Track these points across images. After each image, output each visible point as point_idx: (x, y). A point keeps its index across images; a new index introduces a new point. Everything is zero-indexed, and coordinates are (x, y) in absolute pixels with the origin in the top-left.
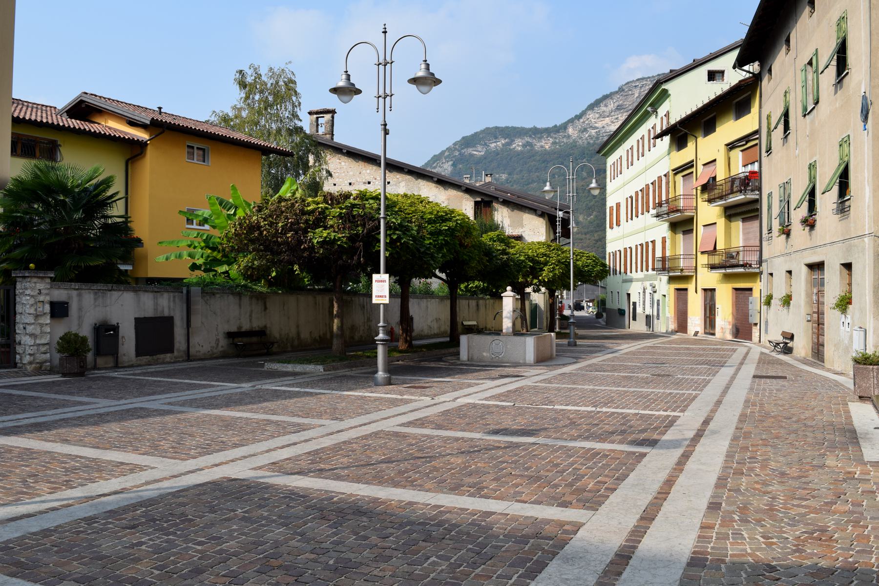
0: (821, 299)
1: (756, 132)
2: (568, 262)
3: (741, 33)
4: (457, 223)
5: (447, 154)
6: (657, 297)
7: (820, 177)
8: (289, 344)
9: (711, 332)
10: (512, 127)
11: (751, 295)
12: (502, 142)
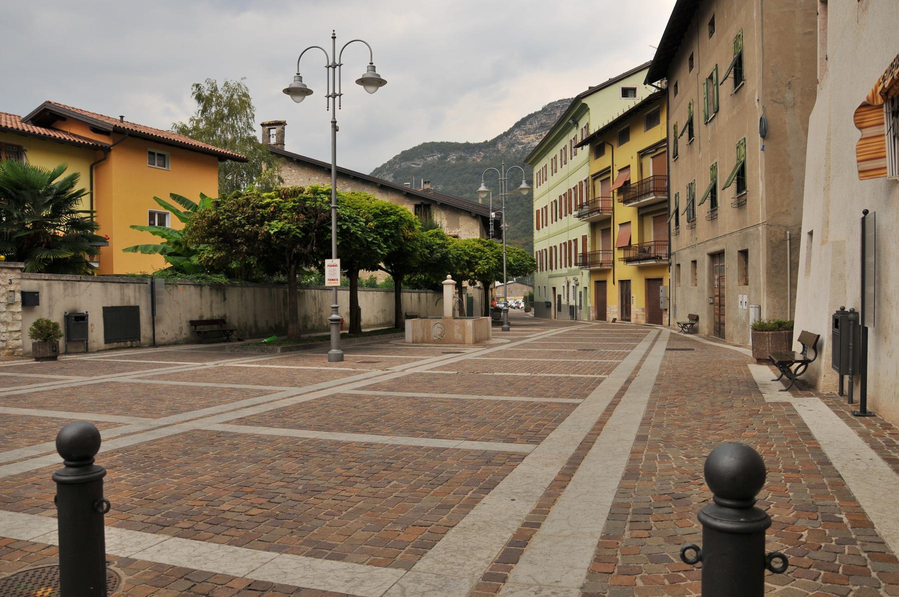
0: (722, 284)
1: (666, 140)
2: (501, 257)
3: (649, 55)
5: (387, 166)
6: (579, 289)
7: (720, 176)
8: (247, 332)
9: (627, 318)
10: (447, 142)
11: (662, 284)
12: (437, 156)
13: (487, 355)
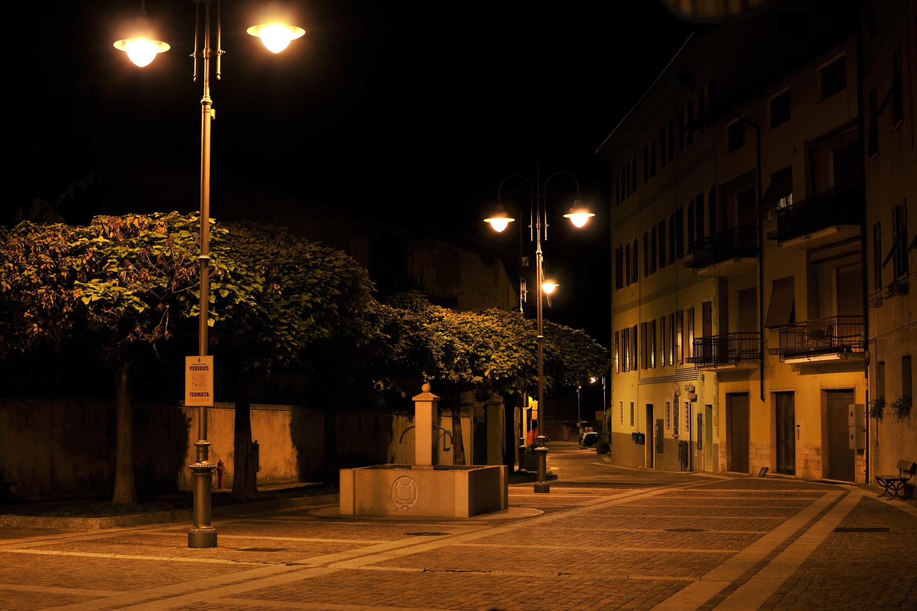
4: (334, 272)
13: (490, 539)
